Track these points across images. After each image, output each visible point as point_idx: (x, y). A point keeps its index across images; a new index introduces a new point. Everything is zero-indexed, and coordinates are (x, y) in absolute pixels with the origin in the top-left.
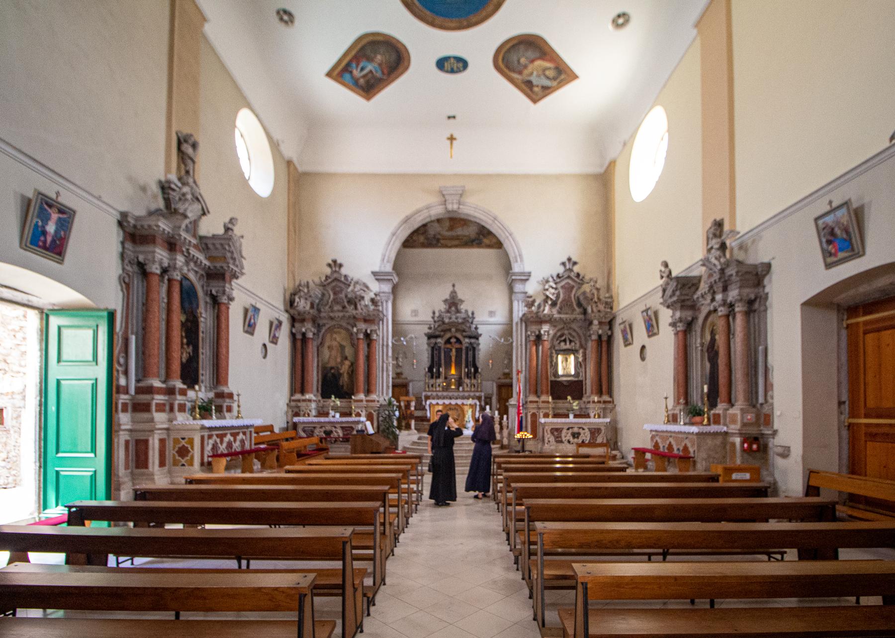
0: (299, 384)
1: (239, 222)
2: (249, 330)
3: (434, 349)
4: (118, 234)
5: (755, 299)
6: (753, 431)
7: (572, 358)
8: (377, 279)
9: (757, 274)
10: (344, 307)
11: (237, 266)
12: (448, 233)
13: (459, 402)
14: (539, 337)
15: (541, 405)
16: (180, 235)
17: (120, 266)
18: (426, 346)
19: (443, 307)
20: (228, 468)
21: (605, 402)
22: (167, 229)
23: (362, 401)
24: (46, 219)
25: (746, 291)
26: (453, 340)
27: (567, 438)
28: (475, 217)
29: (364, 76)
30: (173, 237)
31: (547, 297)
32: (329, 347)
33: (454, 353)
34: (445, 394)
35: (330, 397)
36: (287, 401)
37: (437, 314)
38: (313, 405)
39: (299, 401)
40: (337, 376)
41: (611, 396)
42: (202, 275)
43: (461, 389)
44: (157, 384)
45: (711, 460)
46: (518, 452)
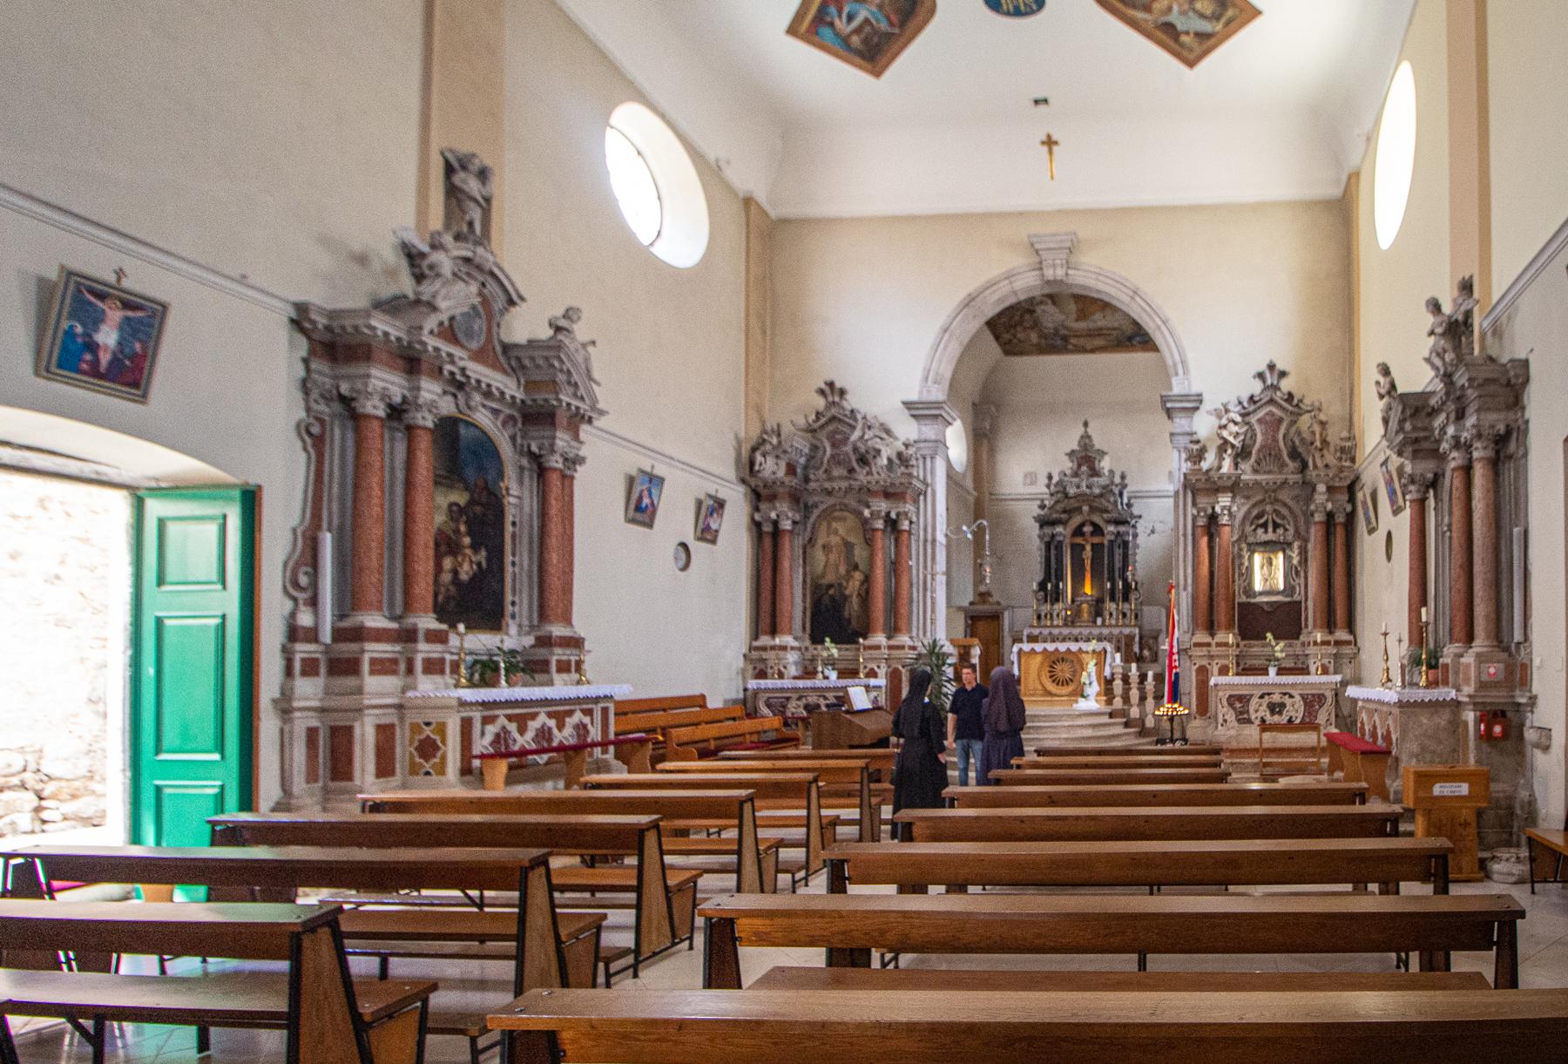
0: (766, 618)
1: (584, 316)
2: (639, 516)
3: (1052, 547)
4: (291, 344)
5: (1509, 432)
6: (1497, 697)
7: (1279, 559)
8: (913, 416)
9: (1508, 384)
10: (851, 471)
11: (582, 398)
12: (1049, 327)
13: (1074, 647)
14: (1213, 518)
15: (1214, 650)
16: (424, 344)
17: (302, 404)
18: (1037, 542)
19: (1068, 465)
20: (510, 781)
21: (1338, 643)
22: (394, 333)
23: (878, 647)
24: (97, 320)
25: (1491, 417)
26: (1087, 529)
27: (1259, 714)
28: (1099, 291)
29: (857, 31)
30: (410, 346)
31: (1226, 441)
32: (824, 547)
33: (1088, 553)
34: (1066, 631)
35: (822, 642)
36: (744, 650)
37: (1056, 479)
38: (792, 657)
39: (764, 649)
40: (839, 602)
41: (1352, 631)
42: (512, 417)
43: (1099, 621)
44: (375, 621)
45: (1428, 757)
46: (1163, 742)
